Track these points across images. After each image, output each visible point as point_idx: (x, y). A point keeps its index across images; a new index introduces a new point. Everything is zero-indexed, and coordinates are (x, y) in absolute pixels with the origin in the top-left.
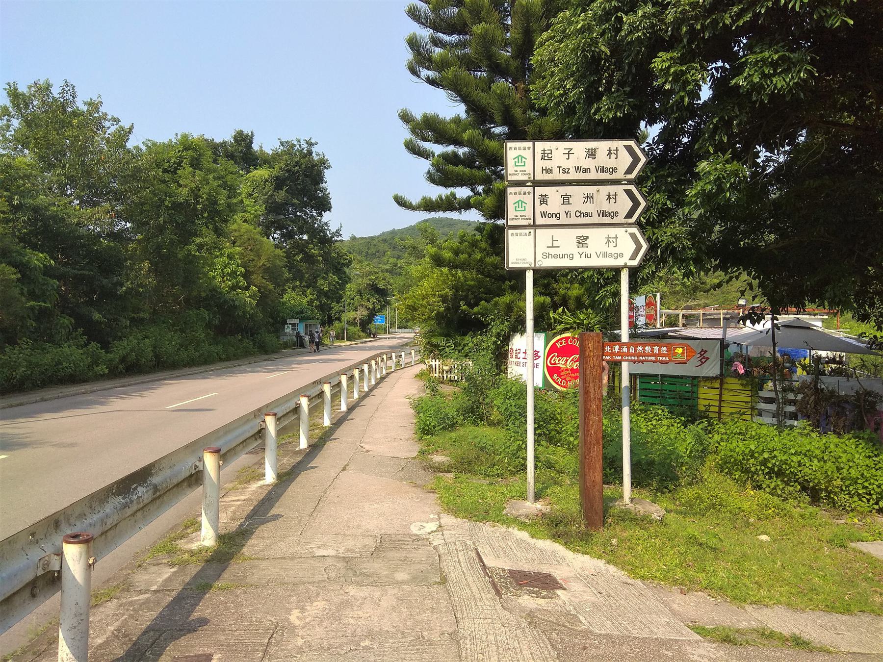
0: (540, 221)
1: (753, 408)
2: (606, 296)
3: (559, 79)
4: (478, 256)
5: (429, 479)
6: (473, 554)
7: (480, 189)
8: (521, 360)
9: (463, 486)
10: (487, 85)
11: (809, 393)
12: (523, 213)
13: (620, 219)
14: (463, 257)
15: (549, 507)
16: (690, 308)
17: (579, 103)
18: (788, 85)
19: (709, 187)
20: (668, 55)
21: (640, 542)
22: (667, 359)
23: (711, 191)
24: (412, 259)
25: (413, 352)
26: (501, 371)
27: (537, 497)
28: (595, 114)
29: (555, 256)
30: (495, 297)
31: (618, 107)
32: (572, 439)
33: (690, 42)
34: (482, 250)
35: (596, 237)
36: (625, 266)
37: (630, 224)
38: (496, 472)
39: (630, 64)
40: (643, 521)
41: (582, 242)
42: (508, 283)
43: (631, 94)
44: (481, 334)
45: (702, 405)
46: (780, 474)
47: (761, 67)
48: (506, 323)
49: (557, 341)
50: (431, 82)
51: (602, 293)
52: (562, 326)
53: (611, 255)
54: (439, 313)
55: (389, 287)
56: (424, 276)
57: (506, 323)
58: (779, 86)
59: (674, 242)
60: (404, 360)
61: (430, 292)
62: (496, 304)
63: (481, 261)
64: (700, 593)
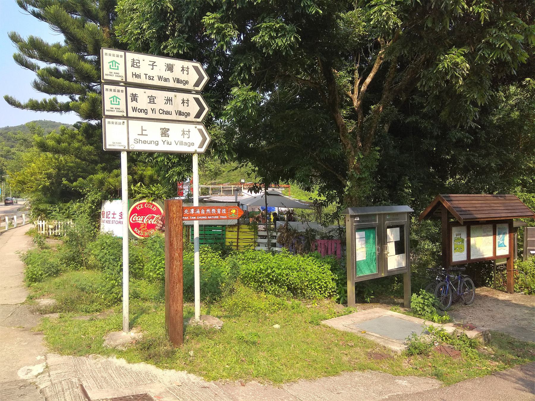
0: (131, 114)
1: (255, 242)
2: (173, 174)
3: (137, 23)
4: (76, 145)
5: (36, 321)
6: (79, 391)
7: (77, 97)
8: (111, 219)
9: (67, 324)
10: (82, 25)
11: (284, 231)
12: (117, 107)
13: (191, 118)
14: (64, 145)
15: (141, 333)
16: (215, 184)
17: (151, 41)
18: (285, 44)
19: (239, 104)
20: (214, 15)
21: (209, 349)
22: (226, 217)
23: (240, 107)
24: (23, 148)
25: (24, 215)
26: (96, 227)
27: (131, 326)
28: (164, 49)
29: (145, 142)
30: (90, 174)
31: (180, 47)
32: (151, 274)
33: (228, 9)
34: (80, 141)
35: (175, 129)
36: (196, 152)
37: (198, 122)
38: (95, 308)
39: (188, 19)
40: (209, 333)
41: (165, 132)
42: (100, 165)
43: (187, 40)
44: (79, 202)
45: (227, 242)
46: (276, 282)
47: (269, 32)
48: (99, 194)
49: (137, 206)
50: (34, 14)
51: (170, 172)
52: (140, 195)
53: (186, 144)
54: (44, 186)
55: (4, 167)
56: (31, 161)
57: (99, 194)
58: (280, 44)
59: (215, 140)
60: (16, 221)
61: (37, 171)
62: (91, 180)
63: (79, 148)
64: (253, 382)
